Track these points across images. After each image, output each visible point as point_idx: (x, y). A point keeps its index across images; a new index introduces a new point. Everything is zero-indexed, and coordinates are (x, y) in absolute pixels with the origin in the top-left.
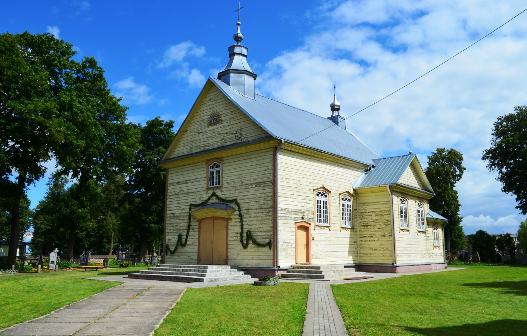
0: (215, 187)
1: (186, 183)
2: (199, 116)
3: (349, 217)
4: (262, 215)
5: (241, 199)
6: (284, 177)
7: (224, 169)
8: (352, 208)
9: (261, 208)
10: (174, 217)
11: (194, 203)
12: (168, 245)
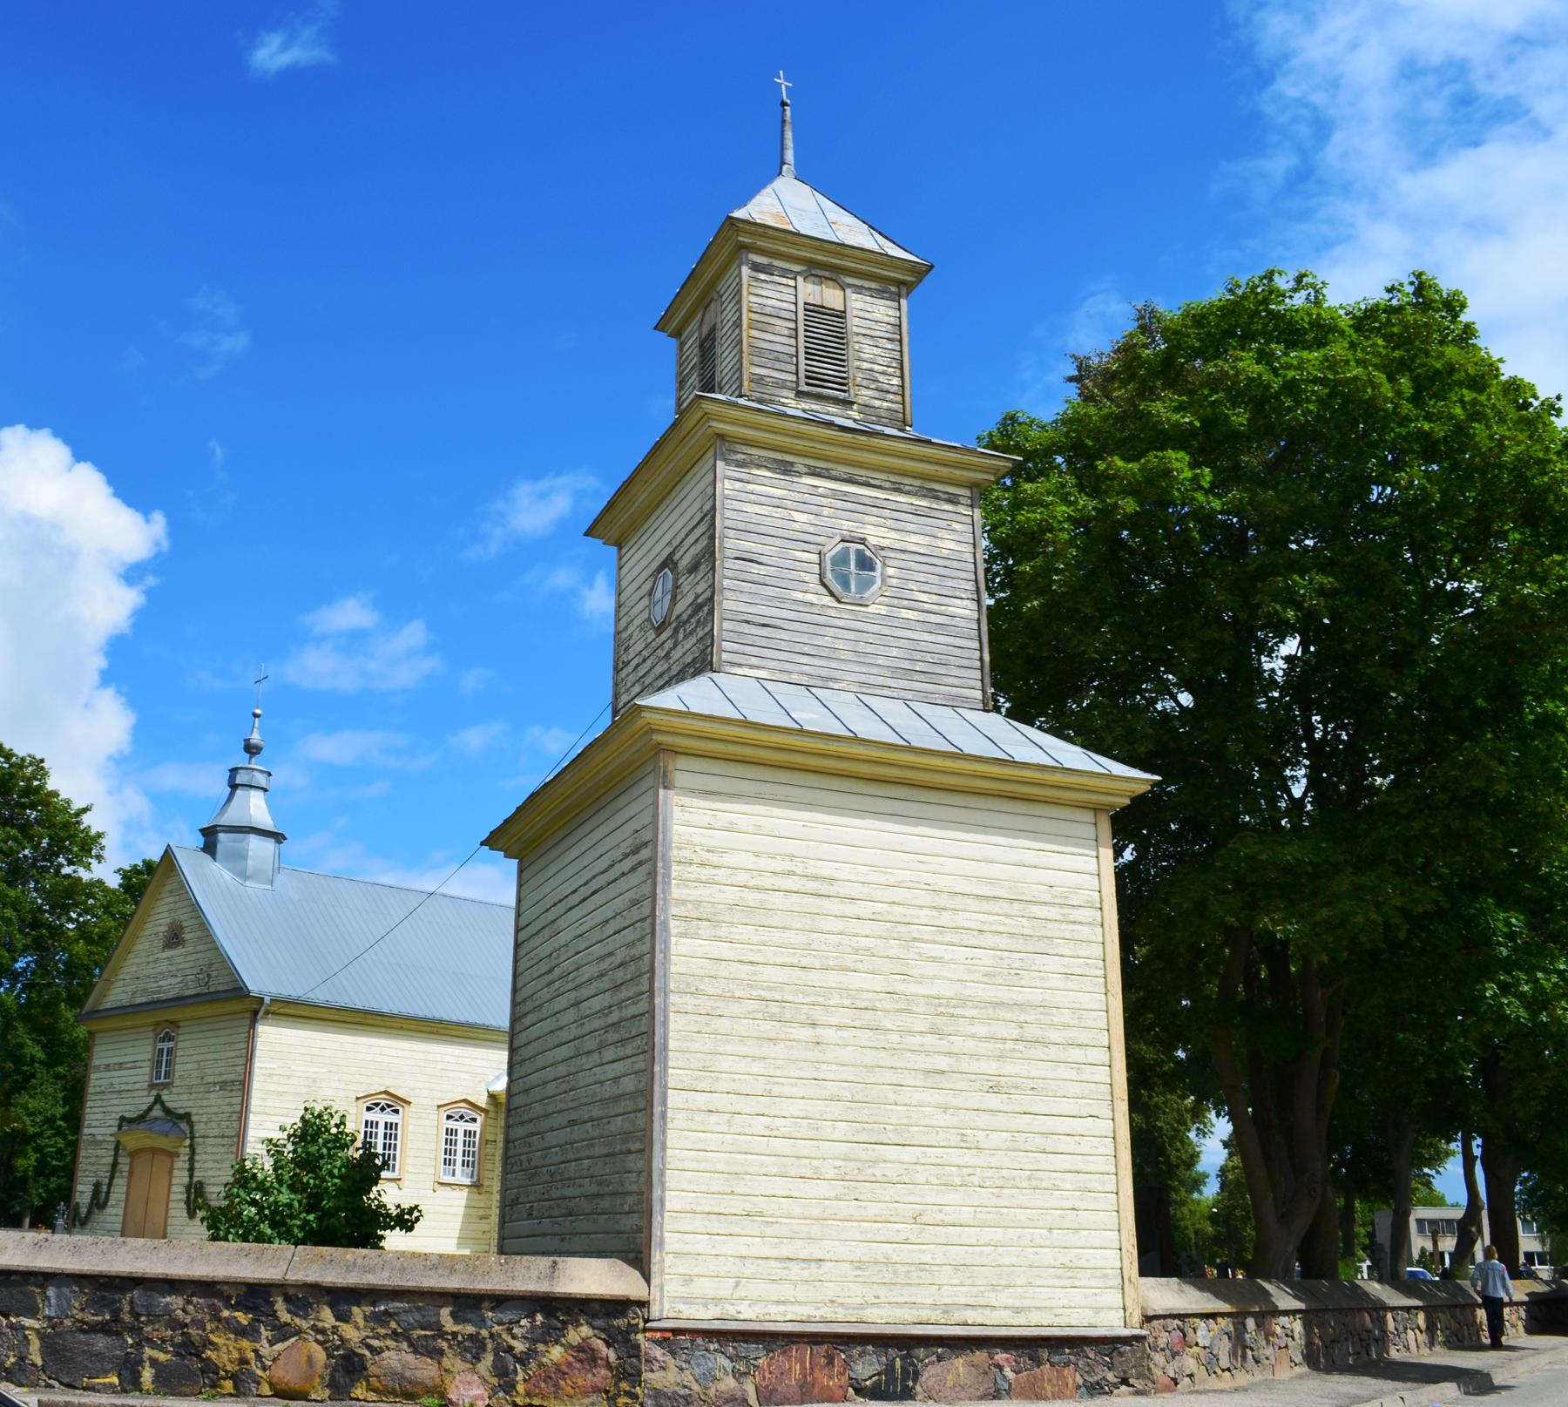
0: (162, 1084)
1: (120, 1069)
2: (152, 924)
3: (448, 1157)
4: (222, 1150)
5: (196, 1114)
6: (275, 1072)
7: (180, 1045)
8: (480, 1139)
9: (223, 1137)
10: (96, 1143)
11: (128, 1115)
12: (78, 1203)
